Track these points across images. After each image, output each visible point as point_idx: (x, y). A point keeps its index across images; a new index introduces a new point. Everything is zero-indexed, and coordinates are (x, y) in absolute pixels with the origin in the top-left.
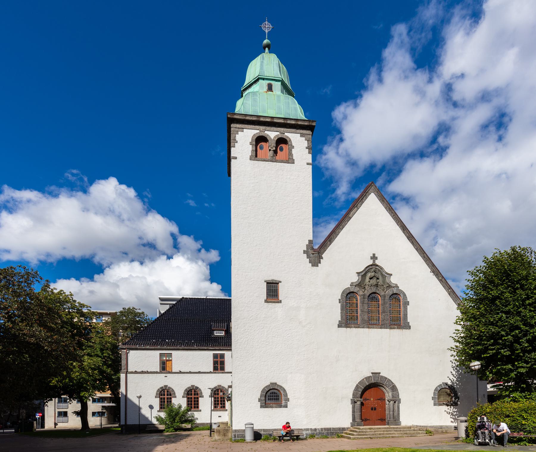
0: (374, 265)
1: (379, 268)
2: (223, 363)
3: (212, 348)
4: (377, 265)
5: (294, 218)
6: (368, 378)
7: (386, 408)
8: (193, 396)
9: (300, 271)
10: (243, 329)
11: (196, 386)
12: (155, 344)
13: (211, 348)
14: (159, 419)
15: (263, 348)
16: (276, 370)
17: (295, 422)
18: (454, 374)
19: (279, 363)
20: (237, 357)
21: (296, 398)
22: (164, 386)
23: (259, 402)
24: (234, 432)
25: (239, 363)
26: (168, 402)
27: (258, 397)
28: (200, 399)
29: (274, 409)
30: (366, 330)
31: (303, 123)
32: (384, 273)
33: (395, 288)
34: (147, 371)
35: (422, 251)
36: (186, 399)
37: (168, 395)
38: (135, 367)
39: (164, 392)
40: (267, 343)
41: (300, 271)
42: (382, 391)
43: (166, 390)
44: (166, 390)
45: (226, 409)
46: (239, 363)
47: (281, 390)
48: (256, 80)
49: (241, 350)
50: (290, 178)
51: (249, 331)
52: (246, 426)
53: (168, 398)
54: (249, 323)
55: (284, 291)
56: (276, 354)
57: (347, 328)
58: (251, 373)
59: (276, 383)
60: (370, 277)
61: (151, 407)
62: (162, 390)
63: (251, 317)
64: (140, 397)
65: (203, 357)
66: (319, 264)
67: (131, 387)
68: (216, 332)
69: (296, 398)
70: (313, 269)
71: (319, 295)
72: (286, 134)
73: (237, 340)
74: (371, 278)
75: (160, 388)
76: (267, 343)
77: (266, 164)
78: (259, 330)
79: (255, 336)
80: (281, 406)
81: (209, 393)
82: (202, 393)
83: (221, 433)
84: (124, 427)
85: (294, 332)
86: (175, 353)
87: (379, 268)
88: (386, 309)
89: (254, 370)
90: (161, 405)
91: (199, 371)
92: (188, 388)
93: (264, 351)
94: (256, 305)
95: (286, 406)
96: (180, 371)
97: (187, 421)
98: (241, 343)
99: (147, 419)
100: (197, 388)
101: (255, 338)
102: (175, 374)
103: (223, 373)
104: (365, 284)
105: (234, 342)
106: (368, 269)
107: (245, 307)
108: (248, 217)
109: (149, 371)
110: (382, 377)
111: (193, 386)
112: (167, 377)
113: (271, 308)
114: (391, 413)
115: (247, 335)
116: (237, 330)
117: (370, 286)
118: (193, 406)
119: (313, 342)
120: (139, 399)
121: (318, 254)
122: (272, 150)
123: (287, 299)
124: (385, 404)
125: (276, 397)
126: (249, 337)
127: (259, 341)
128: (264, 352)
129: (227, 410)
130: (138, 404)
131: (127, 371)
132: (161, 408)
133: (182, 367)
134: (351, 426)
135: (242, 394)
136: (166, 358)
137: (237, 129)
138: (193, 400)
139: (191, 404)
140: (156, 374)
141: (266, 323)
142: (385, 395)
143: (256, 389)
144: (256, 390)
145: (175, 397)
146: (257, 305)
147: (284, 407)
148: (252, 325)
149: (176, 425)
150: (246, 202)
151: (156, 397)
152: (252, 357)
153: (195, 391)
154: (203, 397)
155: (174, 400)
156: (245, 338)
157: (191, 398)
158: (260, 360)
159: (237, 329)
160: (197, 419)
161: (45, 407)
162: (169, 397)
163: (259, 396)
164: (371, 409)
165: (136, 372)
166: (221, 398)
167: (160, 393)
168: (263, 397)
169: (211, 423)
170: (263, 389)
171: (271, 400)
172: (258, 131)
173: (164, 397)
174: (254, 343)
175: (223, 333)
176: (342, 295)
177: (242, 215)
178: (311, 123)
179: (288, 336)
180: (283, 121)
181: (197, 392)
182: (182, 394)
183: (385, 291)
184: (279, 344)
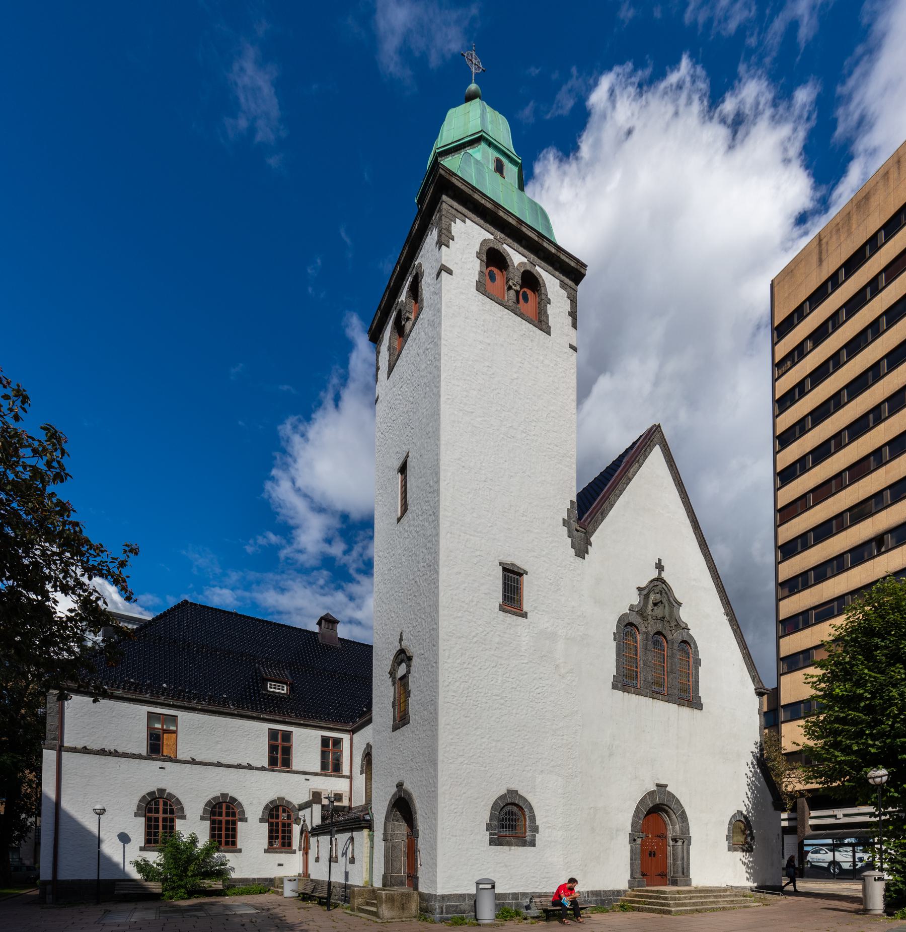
1: (666, 589)
2: (287, 751)
3: (268, 717)
5: (548, 446)
7: (669, 853)
8: (224, 818)
9: (557, 559)
10: (458, 661)
11: (230, 797)
12: (137, 688)
13: (265, 717)
14: (142, 867)
15: (495, 709)
16: (517, 763)
17: (547, 878)
18: (750, 796)
19: (522, 748)
20: (448, 724)
21: (549, 827)
22: (158, 790)
23: (488, 832)
24: (439, 901)
25: (452, 739)
26: (164, 827)
27: (485, 821)
28: (240, 825)
29: (513, 848)
30: (649, 700)
31: (567, 260)
32: (671, 599)
34: (116, 751)
35: (716, 573)
36: (207, 823)
37: (165, 812)
38: (84, 737)
39: (157, 804)
40: (502, 701)
41: (557, 559)
42: (664, 822)
43: (161, 801)
44: (161, 801)
45: (294, 848)
46: (452, 739)
47: (526, 808)
48: (473, 139)
49: (454, 709)
50: (543, 361)
51: (470, 666)
52: (481, 886)
53: (165, 820)
54: (471, 648)
55: (531, 595)
56: (518, 726)
57: (624, 692)
58: (474, 764)
59: (517, 791)
60: (654, 601)
61: (124, 838)
62: (152, 800)
63: (474, 637)
64: (101, 812)
65: (246, 733)
66: (586, 555)
67: (72, 785)
68: (271, 685)
69: (549, 827)
70: (577, 561)
71: (585, 617)
72: (537, 268)
73: (447, 684)
74: (655, 604)
75: (148, 794)
76: (502, 701)
77: (505, 313)
78: (488, 670)
79: (481, 680)
80: (524, 843)
81: (259, 813)
82: (243, 811)
83: (396, 903)
84: (49, 888)
85: (547, 685)
86: (184, 717)
87: (666, 589)
88: (674, 667)
89: (479, 757)
90: (148, 834)
91: (239, 763)
92: (214, 799)
93: (497, 718)
94: (483, 612)
95: (533, 844)
96: (193, 759)
97: (209, 874)
98: (455, 692)
99: (115, 866)
100: (234, 800)
101: (481, 686)
102: (183, 766)
103: (288, 772)
105: (443, 686)
107: (465, 611)
108: (472, 412)
109: (120, 750)
110: (669, 792)
111: (224, 795)
112: (164, 768)
113: (510, 626)
114: (679, 862)
115: (467, 675)
116: (449, 661)
118: (223, 840)
119: (577, 711)
120: (99, 817)
121: (585, 533)
122: (515, 290)
123: (537, 613)
124: (666, 845)
126: (470, 681)
127: (488, 693)
128: (498, 720)
129: (294, 852)
130: (95, 830)
131: (61, 746)
132: (148, 841)
133: (200, 749)
134: (629, 888)
135: (455, 811)
136: (162, 726)
137: (454, 212)
138: (224, 826)
139: (220, 836)
140: (137, 761)
141: (500, 655)
142: (666, 829)
143: (482, 801)
144: (483, 803)
145: (183, 817)
146: (485, 612)
147: (529, 846)
148: (475, 656)
149: (189, 882)
150: (468, 378)
151: (136, 815)
152: (475, 727)
153: (228, 807)
154: (247, 821)
155: (179, 825)
156: (463, 682)
157: (220, 822)
158: (490, 737)
159: (449, 657)
160: (233, 869)
162: (169, 816)
163: (486, 817)
165: (85, 750)
166: (284, 825)
167: (146, 806)
168: (494, 821)
169: (329, 883)
170: (494, 803)
171: (506, 828)
173: (165, 816)
174: (479, 696)
175: (285, 689)
176: (617, 626)
177: (460, 403)
178: (579, 267)
179: (538, 691)
180: (536, 239)
181: (233, 809)
182: (201, 812)
184: (523, 707)
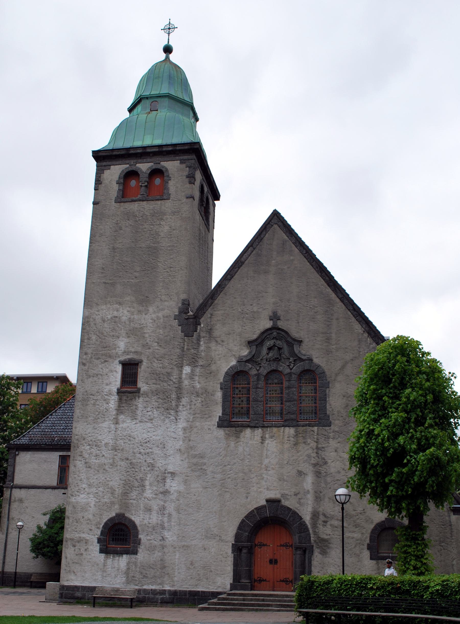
0: (275, 328)
4: (279, 329)
6: (259, 509)
31: (182, 148)
33: (307, 361)
104: (261, 358)
106: (265, 335)
117: (268, 360)
125: (118, 534)
137: (103, 168)
161: (429, 504)
164: (270, 562)
169: (16, 573)
172: (128, 166)
183: (291, 367)
